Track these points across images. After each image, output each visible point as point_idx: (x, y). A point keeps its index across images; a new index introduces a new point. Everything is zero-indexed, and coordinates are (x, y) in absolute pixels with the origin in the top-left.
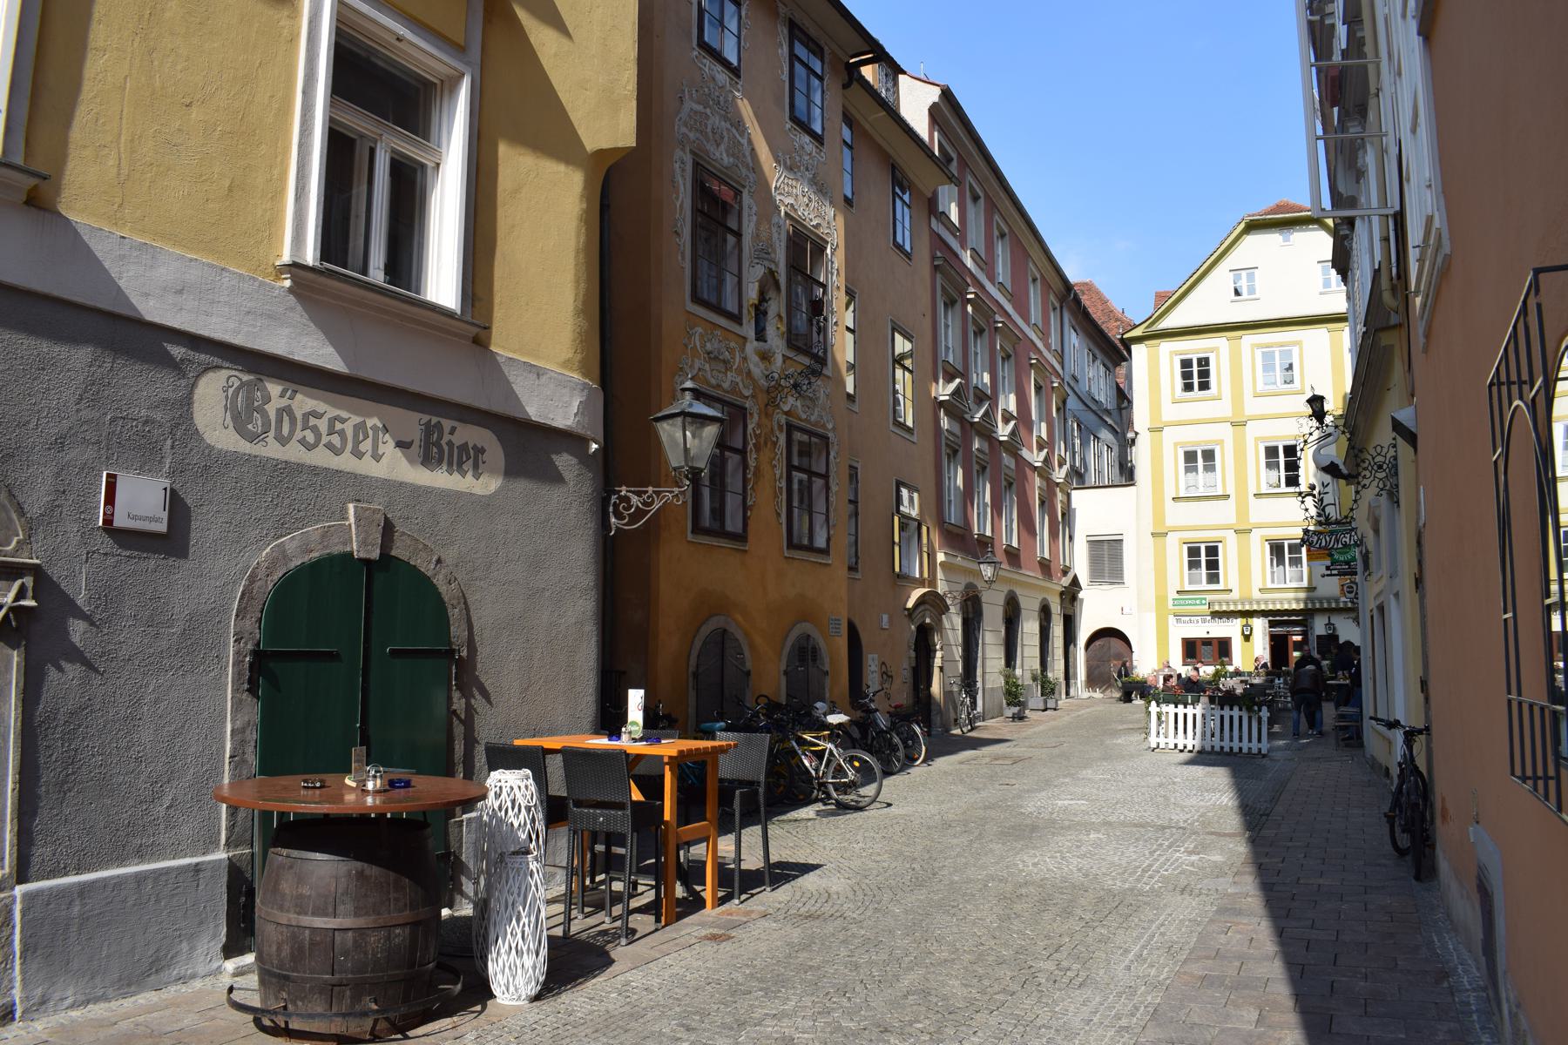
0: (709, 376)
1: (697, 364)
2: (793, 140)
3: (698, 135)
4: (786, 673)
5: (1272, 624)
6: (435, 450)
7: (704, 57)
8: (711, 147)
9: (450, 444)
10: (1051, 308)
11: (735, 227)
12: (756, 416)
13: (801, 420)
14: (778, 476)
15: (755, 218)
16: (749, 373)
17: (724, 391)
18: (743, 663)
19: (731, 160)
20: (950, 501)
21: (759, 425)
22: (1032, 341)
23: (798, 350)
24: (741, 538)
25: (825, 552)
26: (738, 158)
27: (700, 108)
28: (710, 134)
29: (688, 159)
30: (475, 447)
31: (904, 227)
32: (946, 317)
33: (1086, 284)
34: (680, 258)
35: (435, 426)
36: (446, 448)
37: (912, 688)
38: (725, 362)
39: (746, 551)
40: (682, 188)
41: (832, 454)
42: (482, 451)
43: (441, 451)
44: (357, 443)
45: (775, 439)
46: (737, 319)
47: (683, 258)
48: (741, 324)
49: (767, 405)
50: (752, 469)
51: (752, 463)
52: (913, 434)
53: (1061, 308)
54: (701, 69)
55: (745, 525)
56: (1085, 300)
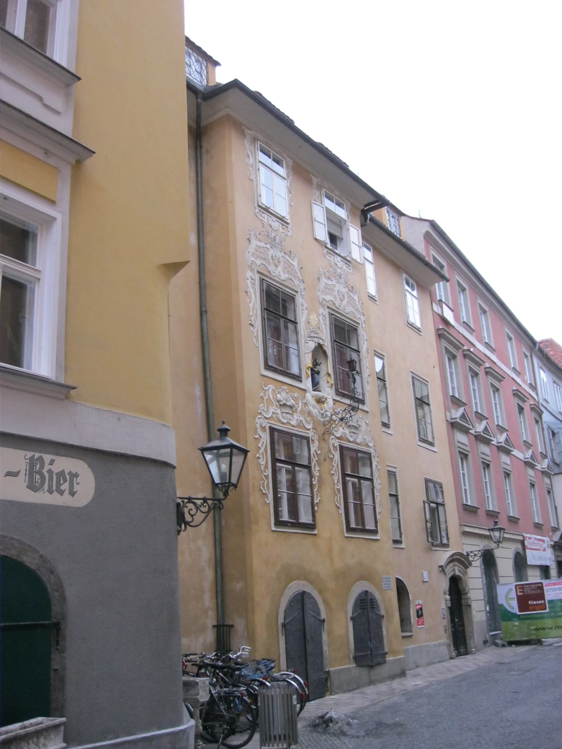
0: (281, 418)
1: (271, 410)
2: (329, 261)
3: (262, 262)
4: (352, 619)
5: (263, 746)
6: (38, 477)
7: (264, 213)
8: (271, 268)
9: (50, 472)
10: (507, 339)
11: (293, 319)
12: (316, 443)
13: (349, 441)
14: (336, 481)
15: (306, 311)
16: (310, 413)
17: (293, 426)
18: (319, 614)
19: (287, 275)
20: (466, 490)
21: (319, 448)
22: (513, 379)
23: (343, 395)
24: (312, 527)
25: (375, 532)
26: (291, 274)
27: (262, 244)
28: (271, 260)
29: (257, 277)
30: (70, 473)
31: (413, 309)
32: (450, 367)
33: (547, 341)
34: (254, 340)
35: (37, 459)
36: (47, 475)
37: (450, 621)
38: (291, 407)
39: (315, 535)
40: (253, 295)
41: (374, 464)
42: (76, 475)
43: (43, 478)
44: (59, 485)
45: (331, 456)
46: (298, 378)
47: (258, 341)
48: (301, 381)
49: (324, 434)
50: (317, 478)
51: (316, 473)
52: (389, 427)
53: (531, 356)
54: (261, 220)
55: (314, 516)
56: (546, 350)
